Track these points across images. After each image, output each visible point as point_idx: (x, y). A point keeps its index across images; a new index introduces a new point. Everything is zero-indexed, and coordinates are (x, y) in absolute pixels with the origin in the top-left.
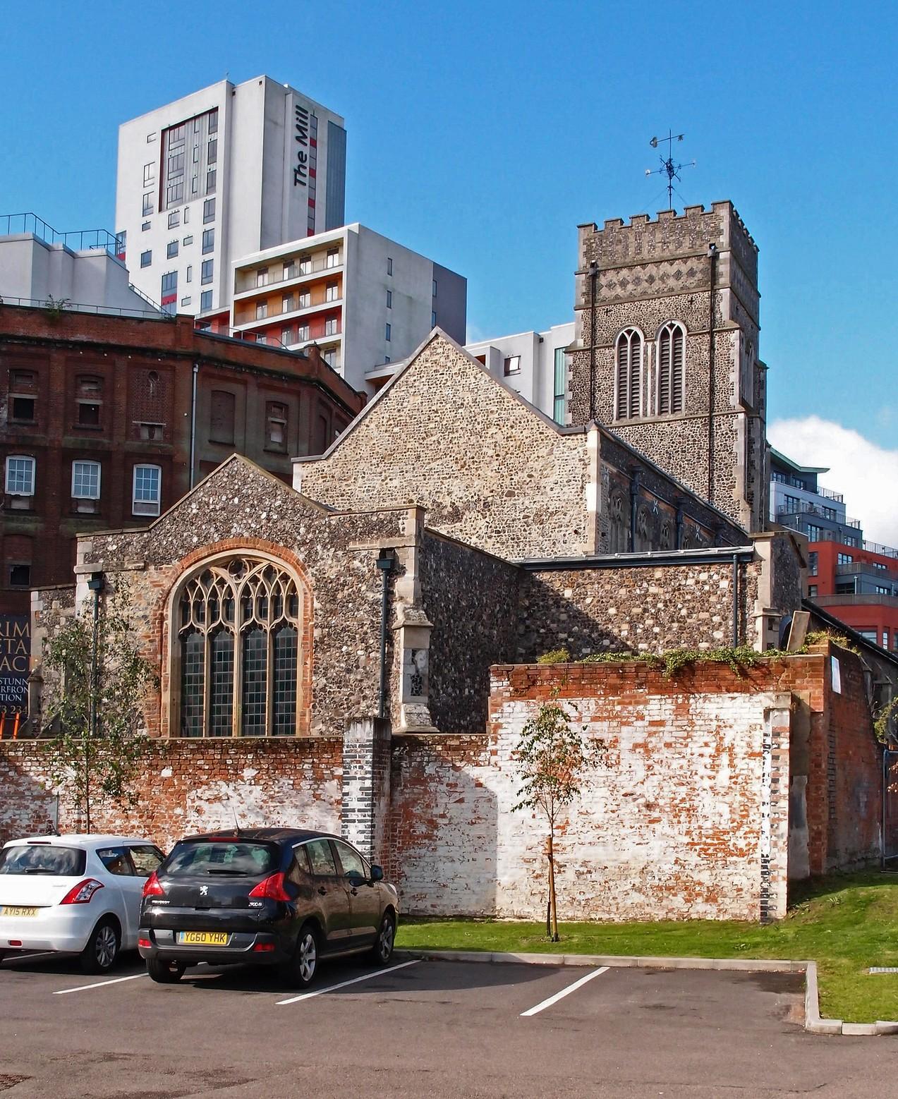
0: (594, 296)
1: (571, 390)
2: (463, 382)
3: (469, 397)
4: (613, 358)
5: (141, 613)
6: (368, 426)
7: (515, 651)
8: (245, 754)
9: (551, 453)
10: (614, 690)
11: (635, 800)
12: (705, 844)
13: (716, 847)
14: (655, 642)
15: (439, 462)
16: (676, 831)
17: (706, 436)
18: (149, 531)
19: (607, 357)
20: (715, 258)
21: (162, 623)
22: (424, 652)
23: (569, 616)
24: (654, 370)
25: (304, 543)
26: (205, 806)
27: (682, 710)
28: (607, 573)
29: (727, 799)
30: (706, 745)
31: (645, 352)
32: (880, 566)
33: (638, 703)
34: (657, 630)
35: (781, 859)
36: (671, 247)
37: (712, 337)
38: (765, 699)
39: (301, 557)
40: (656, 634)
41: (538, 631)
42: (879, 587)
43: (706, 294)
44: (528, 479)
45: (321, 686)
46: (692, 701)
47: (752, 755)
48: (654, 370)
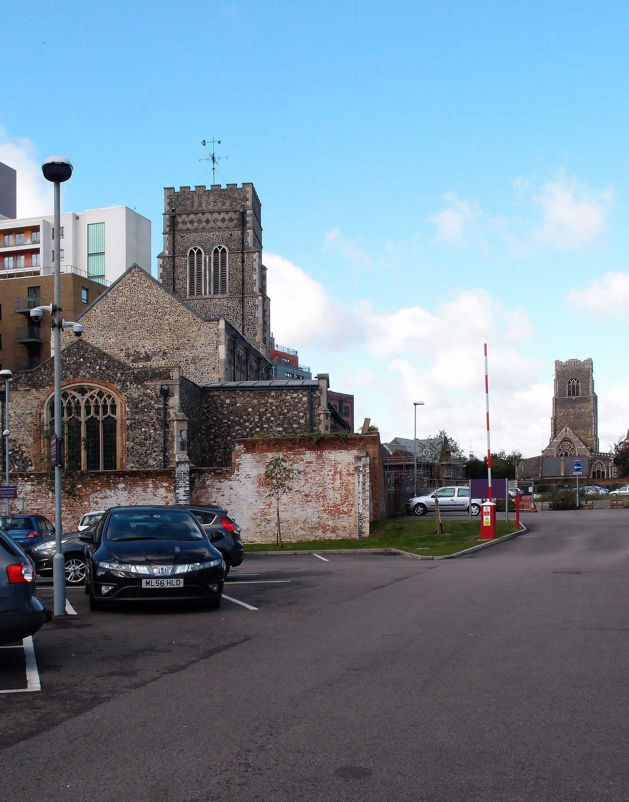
0: (174, 227)
1: (161, 278)
2: (150, 292)
3: (154, 300)
4: (186, 262)
5: (29, 412)
6: (95, 311)
7: (201, 427)
8: (119, 477)
9: (199, 329)
10: (290, 449)
11: (300, 493)
12: (330, 510)
13: (335, 511)
14: (271, 424)
15: (137, 331)
16: (318, 505)
17: (240, 307)
18: (32, 372)
19: (183, 262)
20: (243, 214)
21: (40, 416)
22: (185, 432)
23: (228, 412)
24: (210, 270)
25: (120, 381)
26: (100, 501)
27: (320, 457)
28: (247, 393)
29: (339, 492)
30: (330, 471)
31: (205, 261)
32: (286, 360)
33: (301, 454)
34: (272, 419)
35: (367, 514)
36: (219, 205)
37: (243, 255)
38: (355, 452)
39: (119, 387)
40: (272, 420)
41: (212, 419)
42: (287, 373)
43: (239, 232)
44: (187, 342)
45: (131, 446)
46: (323, 453)
47: (350, 475)
48: (210, 270)
